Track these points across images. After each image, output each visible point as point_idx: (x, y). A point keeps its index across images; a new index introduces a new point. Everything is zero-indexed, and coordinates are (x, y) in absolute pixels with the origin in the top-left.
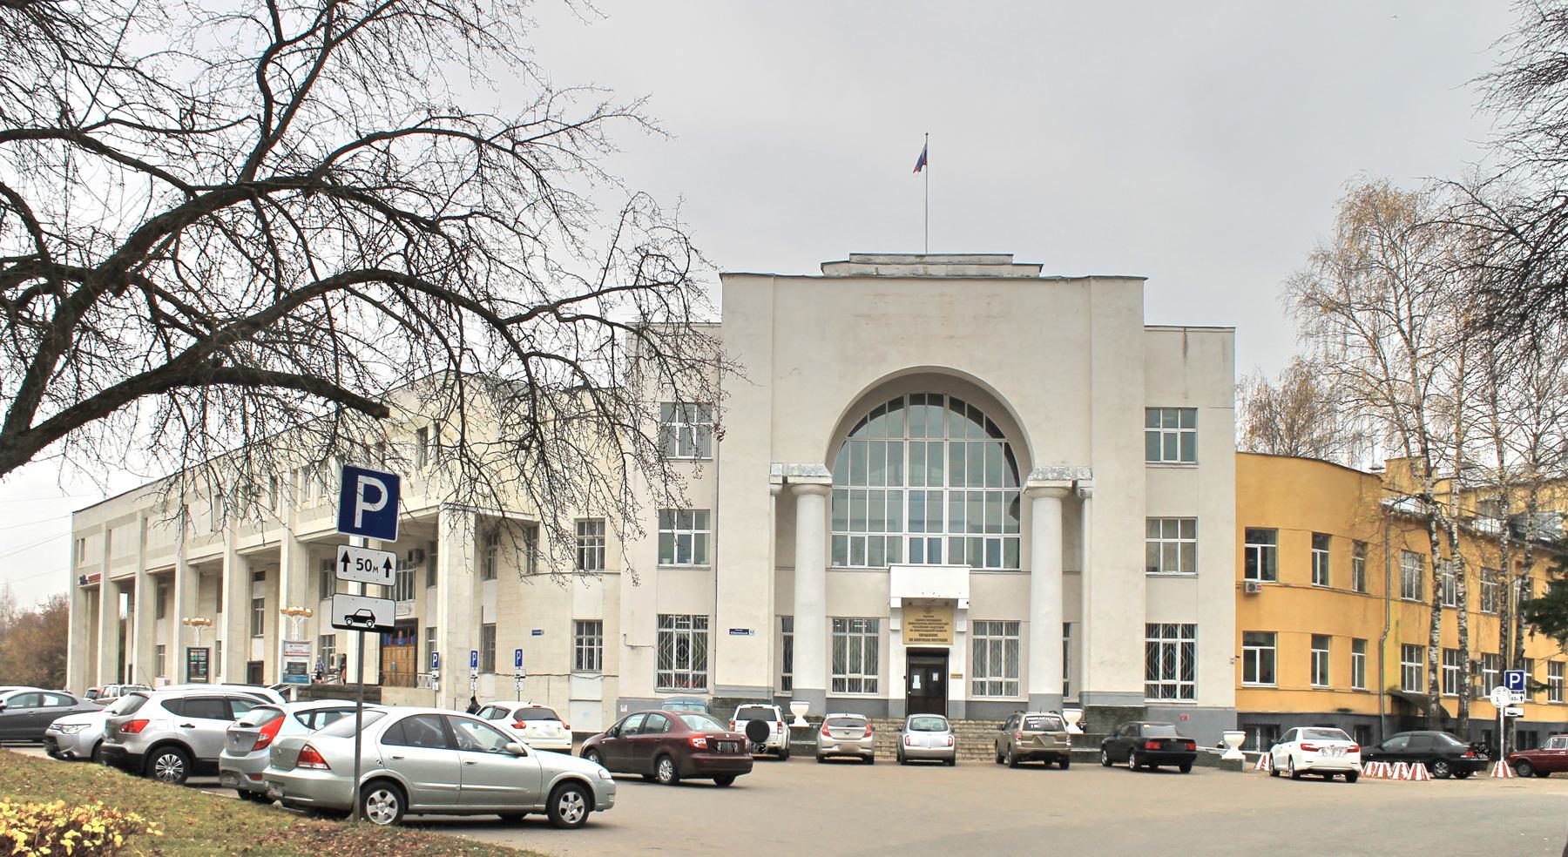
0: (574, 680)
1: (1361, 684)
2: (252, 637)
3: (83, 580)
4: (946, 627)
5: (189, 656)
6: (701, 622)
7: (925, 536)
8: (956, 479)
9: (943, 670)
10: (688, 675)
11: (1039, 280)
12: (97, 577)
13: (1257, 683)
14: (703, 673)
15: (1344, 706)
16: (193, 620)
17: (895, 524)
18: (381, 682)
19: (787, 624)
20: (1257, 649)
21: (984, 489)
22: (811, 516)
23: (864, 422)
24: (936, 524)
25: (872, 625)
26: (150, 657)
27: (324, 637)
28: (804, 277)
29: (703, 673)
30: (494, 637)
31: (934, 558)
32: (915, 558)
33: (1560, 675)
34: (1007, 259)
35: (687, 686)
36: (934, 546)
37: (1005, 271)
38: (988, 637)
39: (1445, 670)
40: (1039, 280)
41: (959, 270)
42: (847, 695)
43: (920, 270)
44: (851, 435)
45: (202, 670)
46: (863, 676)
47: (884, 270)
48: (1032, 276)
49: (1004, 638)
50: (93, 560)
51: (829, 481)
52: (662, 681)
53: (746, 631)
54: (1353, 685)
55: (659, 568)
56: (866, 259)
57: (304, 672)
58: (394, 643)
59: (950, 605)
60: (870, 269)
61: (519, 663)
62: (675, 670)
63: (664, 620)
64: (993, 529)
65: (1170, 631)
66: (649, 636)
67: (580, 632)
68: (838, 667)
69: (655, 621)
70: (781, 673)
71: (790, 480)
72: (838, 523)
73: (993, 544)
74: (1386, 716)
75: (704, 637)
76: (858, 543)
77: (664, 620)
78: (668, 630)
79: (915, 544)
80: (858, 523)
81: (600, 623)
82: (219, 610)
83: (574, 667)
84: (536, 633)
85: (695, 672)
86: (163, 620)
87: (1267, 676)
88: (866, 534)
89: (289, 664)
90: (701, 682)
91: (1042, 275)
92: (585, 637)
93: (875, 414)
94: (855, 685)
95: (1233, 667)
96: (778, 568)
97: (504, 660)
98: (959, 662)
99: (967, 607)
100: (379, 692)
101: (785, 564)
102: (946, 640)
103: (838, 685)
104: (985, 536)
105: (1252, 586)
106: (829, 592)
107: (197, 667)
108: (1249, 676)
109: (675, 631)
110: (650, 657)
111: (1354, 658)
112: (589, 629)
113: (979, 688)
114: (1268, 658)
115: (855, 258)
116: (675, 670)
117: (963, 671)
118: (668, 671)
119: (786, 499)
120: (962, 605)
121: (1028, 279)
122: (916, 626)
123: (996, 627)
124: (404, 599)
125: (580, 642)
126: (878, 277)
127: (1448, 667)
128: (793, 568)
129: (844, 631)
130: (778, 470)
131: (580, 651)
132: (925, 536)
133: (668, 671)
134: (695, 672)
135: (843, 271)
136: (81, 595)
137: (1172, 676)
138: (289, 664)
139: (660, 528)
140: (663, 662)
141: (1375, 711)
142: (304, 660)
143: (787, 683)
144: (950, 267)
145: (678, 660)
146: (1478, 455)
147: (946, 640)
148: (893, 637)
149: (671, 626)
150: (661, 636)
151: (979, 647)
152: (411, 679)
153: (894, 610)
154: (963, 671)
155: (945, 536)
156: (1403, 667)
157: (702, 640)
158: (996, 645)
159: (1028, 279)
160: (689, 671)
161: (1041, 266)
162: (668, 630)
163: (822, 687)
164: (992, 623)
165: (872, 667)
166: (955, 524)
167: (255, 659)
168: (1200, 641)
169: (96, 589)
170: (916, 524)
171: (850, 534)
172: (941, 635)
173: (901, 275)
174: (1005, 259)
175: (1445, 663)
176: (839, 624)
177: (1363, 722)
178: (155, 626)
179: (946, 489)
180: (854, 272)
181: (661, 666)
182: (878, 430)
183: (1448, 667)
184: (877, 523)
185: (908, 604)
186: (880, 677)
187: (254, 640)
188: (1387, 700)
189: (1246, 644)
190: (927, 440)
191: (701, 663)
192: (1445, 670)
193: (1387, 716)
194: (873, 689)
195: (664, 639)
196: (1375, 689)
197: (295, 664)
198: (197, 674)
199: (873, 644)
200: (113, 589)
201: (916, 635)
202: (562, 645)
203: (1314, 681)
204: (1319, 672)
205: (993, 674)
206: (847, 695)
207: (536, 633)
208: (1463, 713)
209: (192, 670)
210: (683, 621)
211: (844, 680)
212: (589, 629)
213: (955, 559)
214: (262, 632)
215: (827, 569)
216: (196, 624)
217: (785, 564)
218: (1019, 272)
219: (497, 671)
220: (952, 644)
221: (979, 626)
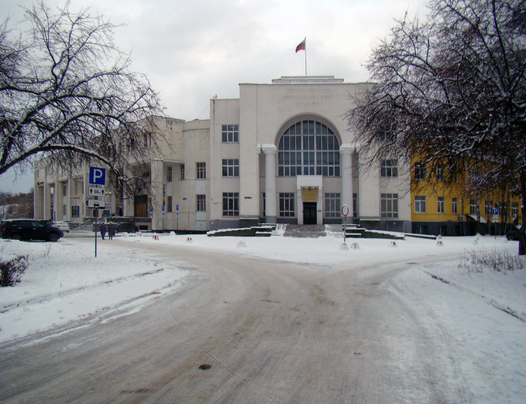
3: (38, 184)
7: (309, 166)
8: (319, 148)
9: (315, 208)
12: (43, 183)
16: (74, 197)
17: (299, 162)
19: (263, 195)
20: (420, 201)
21: (328, 151)
24: (312, 162)
26: (61, 209)
30: (171, 200)
31: (312, 173)
32: (306, 173)
33: (517, 207)
36: (312, 169)
39: (512, 209)
42: (285, 217)
45: (77, 213)
46: (289, 211)
50: (41, 179)
52: (225, 214)
53: (250, 198)
57: (109, 213)
61: (178, 209)
63: (225, 194)
64: (331, 163)
65: (389, 196)
66: (220, 199)
68: (281, 208)
69: (222, 195)
72: (280, 162)
73: (331, 169)
76: (331, 169)
77: (225, 194)
78: (226, 197)
79: (306, 169)
80: (287, 162)
82: (83, 193)
83: (197, 209)
84: (185, 199)
86: (65, 196)
87: (424, 210)
88: (290, 166)
90: (237, 214)
91: (343, 82)
94: (287, 214)
95: (410, 207)
97: (174, 208)
98: (320, 206)
101: (262, 175)
103: (282, 214)
104: (328, 166)
106: (277, 184)
107: (75, 212)
108: (417, 209)
111: (453, 204)
112: (201, 198)
114: (424, 204)
116: (229, 210)
117: (321, 209)
119: (262, 156)
123: (333, 195)
127: (513, 208)
130: (259, 146)
132: (309, 166)
136: (38, 189)
137: (390, 210)
139: (279, 164)
140: (225, 207)
142: (109, 209)
143: (264, 213)
146: (20, 163)
149: (227, 196)
150: (224, 199)
151: (327, 202)
152: (146, 214)
154: (321, 209)
155: (315, 166)
156: (471, 207)
157: (237, 201)
158: (332, 201)
160: (233, 211)
162: (226, 197)
164: (331, 194)
165: (292, 208)
166: (319, 162)
169: (43, 187)
170: (306, 162)
171: (284, 166)
176: (281, 195)
178: (62, 198)
179: (315, 151)
181: (224, 209)
183: (513, 208)
184: (293, 162)
190: (309, 135)
191: (237, 208)
192: (512, 209)
193: (465, 223)
195: (225, 201)
198: (75, 214)
200: (48, 187)
202: (193, 202)
204: (441, 209)
205: (332, 210)
206: (285, 217)
207: (185, 199)
208: (489, 221)
209: (74, 213)
210: (231, 195)
212: (201, 198)
213: (319, 173)
216: (75, 198)
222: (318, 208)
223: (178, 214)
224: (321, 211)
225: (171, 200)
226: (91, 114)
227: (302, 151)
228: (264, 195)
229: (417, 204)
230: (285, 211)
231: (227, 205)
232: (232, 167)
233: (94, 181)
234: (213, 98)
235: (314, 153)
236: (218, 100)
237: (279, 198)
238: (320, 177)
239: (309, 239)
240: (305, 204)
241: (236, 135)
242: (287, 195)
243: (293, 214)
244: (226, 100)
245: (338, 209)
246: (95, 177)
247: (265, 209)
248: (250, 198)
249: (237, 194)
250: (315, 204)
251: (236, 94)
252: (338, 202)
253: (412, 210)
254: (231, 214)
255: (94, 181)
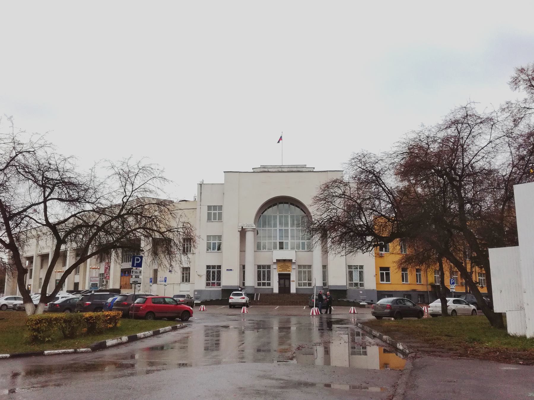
0: (181, 285)
1: (420, 282)
2: (75, 275)
4: (290, 267)
5: (56, 282)
6: (219, 267)
10: (215, 283)
11: (313, 172)
13: (385, 282)
14: (219, 282)
15: (414, 289)
18: (120, 288)
20: (385, 272)
22: (250, 236)
23: (266, 210)
25: (269, 267)
27: (101, 274)
28: (247, 172)
29: (219, 282)
34: (305, 166)
35: (215, 286)
37: (304, 170)
38: (302, 270)
40: (313, 172)
41: (291, 169)
42: (262, 287)
43: (280, 170)
44: (262, 214)
46: (266, 282)
47: (270, 170)
48: (312, 171)
49: (307, 270)
51: (255, 228)
52: (208, 284)
53: (231, 270)
54: (417, 282)
55: (207, 252)
56: (264, 167)
58: (124, 275)
59: (290, 261)
60: (266, 170)
62: (211, 281)
63: (208, 267)
66: (204, 272)
67: (183, 271)
69: (205, 267)
70: (242, 281)
71: (244, 228)
74: (429, 291)
75: (220, 271)
77: (208, 267)
81: (189, 268)
83: (182, 281)
85: (217, 282)
87: (388, 280)
89: (92, 284)
90: (219, 284)
91: (314, 170)
92: (185, 272)
93: (269, 208)
94: (264, 284)
95: (375, 277)
96: (241, 251)
98: (293, 277)
99: (295, 262)
100: (120, 291)
101: (242, 250)
102: (289, 271)
103: (259, 284)
105: (381, 254)
106: (255, 258)
108: (382, 280)
109: (211, 270)
110: (204, 278)
111: (417, 274)
113: (300, 285)
114: (388, 274)
115: (262, 167)
117: (295, 280)
118: (209, 282)
119: (243, 232)
120: (293, 261)
121: (310, 171)
122: (281, 267)
124: (128, 262)
125: (183, 274)
126: (268, 172)
127: (480, 278)
128: (245, 251)
129: (261, 269)
131: (183, 277)
133: (209, 282)
134: (217, 282)
135: (259, 170)
138: (92, 284)
140: (208, 279)
141: (426, 290)
143: (244, 284)
144: (288, 169)
145: (212, 278)
147: (289, 271)
148: (274, 270)
150: (207, 271)
151: (300, 272)
153: (274, 263)
154: (295, 280)
157: (219, 273)
159: (310, 171)
160: (216, 281)
161: (314, 168)
163: (253, 285)
165: (269, 279)
167: (76, 281)
168: (365, 270)
172: (288, 270)
173: (275, 171)
174: (304, 167)
175: (479, 277)
176: (259, 267)
177: (421, 293)
178: (40, 270)
179: (289, 228)
180: (262, 170)
181: (207, 280)
182: (270, 212)
185: (278, 261)
186: (271, 282)
187: (76, 276)
188: (429, 287)
189: (311, 271)
191: (219, 278)
194: (270, 285)
195: (208, 273)
196: (425, 283)
197: (94, 284)
199: (269, 272)
201: (281, 270)
203: (403, 281)
210: (214, 267)
211: (261, 283)
213: (292, 248)
214: (79, 273)
215: (255, 251)
217: (242, 250)
218: (307, 170)
219: (158, 283)
220: (291, 272)
221: (300, 266)
222: (292, 279)
223: (165, 285)
224: (294, 281)
225: (157, 272)
226: (149, 233)
227: (278, 228)
228: (244, 267)
229: (382, 274)
230: (262, 281)
231: (210, 277)
232: (216, 243)
233: (135, 265)
234: (200, 183)
235: (288, 230)
236: (204, 184)
237: (257, 270)
238: (293, 252)
239: (232, 285)
240: (280, 275)
241: (220, 215)
242: (264, 267)
243: (269, 284)
244: (213, 184)
245: (310, 279)
246: (136, 262)
247: (244, 280)
248: (231, 270)
249: (219, 267)
250: (289, 275)
251: (220, 179)
252: (310, 273)
253: (377, 280)
254: (213, 284)
255: (135, 265)
